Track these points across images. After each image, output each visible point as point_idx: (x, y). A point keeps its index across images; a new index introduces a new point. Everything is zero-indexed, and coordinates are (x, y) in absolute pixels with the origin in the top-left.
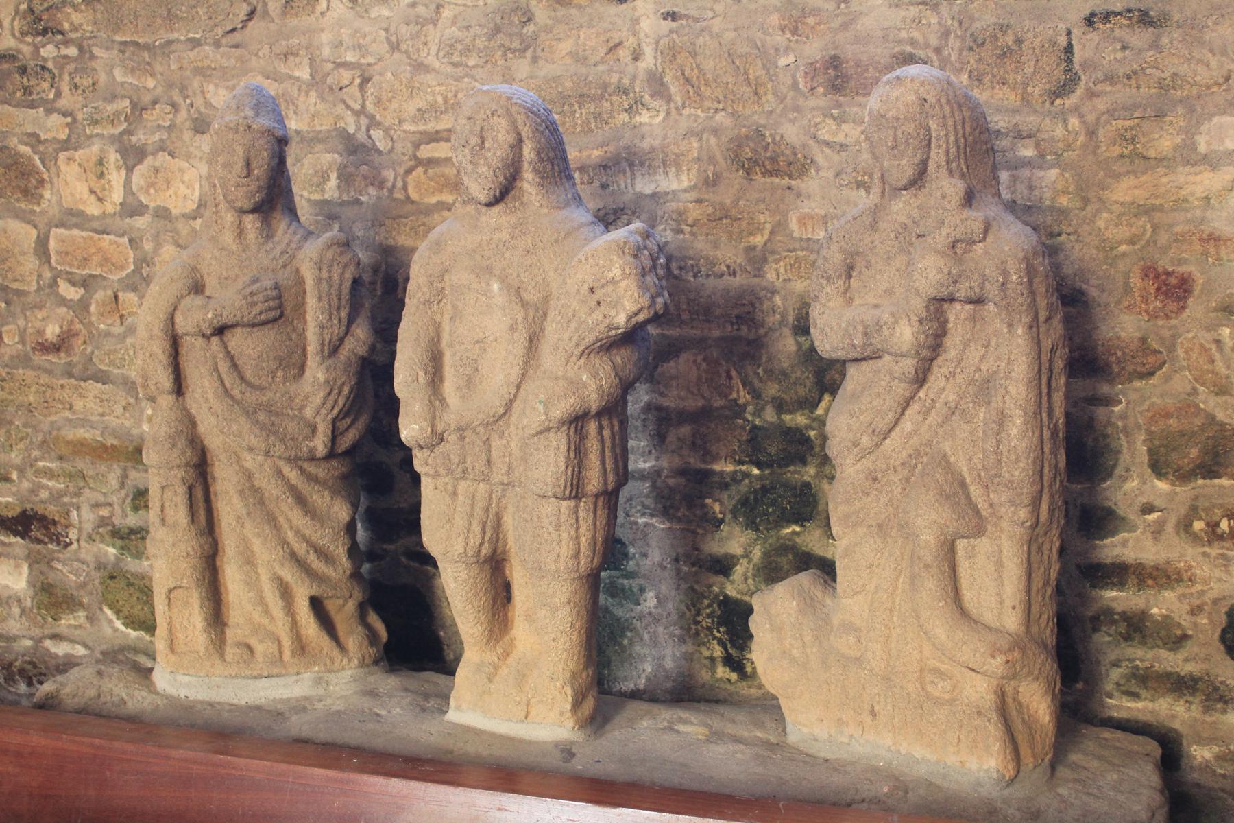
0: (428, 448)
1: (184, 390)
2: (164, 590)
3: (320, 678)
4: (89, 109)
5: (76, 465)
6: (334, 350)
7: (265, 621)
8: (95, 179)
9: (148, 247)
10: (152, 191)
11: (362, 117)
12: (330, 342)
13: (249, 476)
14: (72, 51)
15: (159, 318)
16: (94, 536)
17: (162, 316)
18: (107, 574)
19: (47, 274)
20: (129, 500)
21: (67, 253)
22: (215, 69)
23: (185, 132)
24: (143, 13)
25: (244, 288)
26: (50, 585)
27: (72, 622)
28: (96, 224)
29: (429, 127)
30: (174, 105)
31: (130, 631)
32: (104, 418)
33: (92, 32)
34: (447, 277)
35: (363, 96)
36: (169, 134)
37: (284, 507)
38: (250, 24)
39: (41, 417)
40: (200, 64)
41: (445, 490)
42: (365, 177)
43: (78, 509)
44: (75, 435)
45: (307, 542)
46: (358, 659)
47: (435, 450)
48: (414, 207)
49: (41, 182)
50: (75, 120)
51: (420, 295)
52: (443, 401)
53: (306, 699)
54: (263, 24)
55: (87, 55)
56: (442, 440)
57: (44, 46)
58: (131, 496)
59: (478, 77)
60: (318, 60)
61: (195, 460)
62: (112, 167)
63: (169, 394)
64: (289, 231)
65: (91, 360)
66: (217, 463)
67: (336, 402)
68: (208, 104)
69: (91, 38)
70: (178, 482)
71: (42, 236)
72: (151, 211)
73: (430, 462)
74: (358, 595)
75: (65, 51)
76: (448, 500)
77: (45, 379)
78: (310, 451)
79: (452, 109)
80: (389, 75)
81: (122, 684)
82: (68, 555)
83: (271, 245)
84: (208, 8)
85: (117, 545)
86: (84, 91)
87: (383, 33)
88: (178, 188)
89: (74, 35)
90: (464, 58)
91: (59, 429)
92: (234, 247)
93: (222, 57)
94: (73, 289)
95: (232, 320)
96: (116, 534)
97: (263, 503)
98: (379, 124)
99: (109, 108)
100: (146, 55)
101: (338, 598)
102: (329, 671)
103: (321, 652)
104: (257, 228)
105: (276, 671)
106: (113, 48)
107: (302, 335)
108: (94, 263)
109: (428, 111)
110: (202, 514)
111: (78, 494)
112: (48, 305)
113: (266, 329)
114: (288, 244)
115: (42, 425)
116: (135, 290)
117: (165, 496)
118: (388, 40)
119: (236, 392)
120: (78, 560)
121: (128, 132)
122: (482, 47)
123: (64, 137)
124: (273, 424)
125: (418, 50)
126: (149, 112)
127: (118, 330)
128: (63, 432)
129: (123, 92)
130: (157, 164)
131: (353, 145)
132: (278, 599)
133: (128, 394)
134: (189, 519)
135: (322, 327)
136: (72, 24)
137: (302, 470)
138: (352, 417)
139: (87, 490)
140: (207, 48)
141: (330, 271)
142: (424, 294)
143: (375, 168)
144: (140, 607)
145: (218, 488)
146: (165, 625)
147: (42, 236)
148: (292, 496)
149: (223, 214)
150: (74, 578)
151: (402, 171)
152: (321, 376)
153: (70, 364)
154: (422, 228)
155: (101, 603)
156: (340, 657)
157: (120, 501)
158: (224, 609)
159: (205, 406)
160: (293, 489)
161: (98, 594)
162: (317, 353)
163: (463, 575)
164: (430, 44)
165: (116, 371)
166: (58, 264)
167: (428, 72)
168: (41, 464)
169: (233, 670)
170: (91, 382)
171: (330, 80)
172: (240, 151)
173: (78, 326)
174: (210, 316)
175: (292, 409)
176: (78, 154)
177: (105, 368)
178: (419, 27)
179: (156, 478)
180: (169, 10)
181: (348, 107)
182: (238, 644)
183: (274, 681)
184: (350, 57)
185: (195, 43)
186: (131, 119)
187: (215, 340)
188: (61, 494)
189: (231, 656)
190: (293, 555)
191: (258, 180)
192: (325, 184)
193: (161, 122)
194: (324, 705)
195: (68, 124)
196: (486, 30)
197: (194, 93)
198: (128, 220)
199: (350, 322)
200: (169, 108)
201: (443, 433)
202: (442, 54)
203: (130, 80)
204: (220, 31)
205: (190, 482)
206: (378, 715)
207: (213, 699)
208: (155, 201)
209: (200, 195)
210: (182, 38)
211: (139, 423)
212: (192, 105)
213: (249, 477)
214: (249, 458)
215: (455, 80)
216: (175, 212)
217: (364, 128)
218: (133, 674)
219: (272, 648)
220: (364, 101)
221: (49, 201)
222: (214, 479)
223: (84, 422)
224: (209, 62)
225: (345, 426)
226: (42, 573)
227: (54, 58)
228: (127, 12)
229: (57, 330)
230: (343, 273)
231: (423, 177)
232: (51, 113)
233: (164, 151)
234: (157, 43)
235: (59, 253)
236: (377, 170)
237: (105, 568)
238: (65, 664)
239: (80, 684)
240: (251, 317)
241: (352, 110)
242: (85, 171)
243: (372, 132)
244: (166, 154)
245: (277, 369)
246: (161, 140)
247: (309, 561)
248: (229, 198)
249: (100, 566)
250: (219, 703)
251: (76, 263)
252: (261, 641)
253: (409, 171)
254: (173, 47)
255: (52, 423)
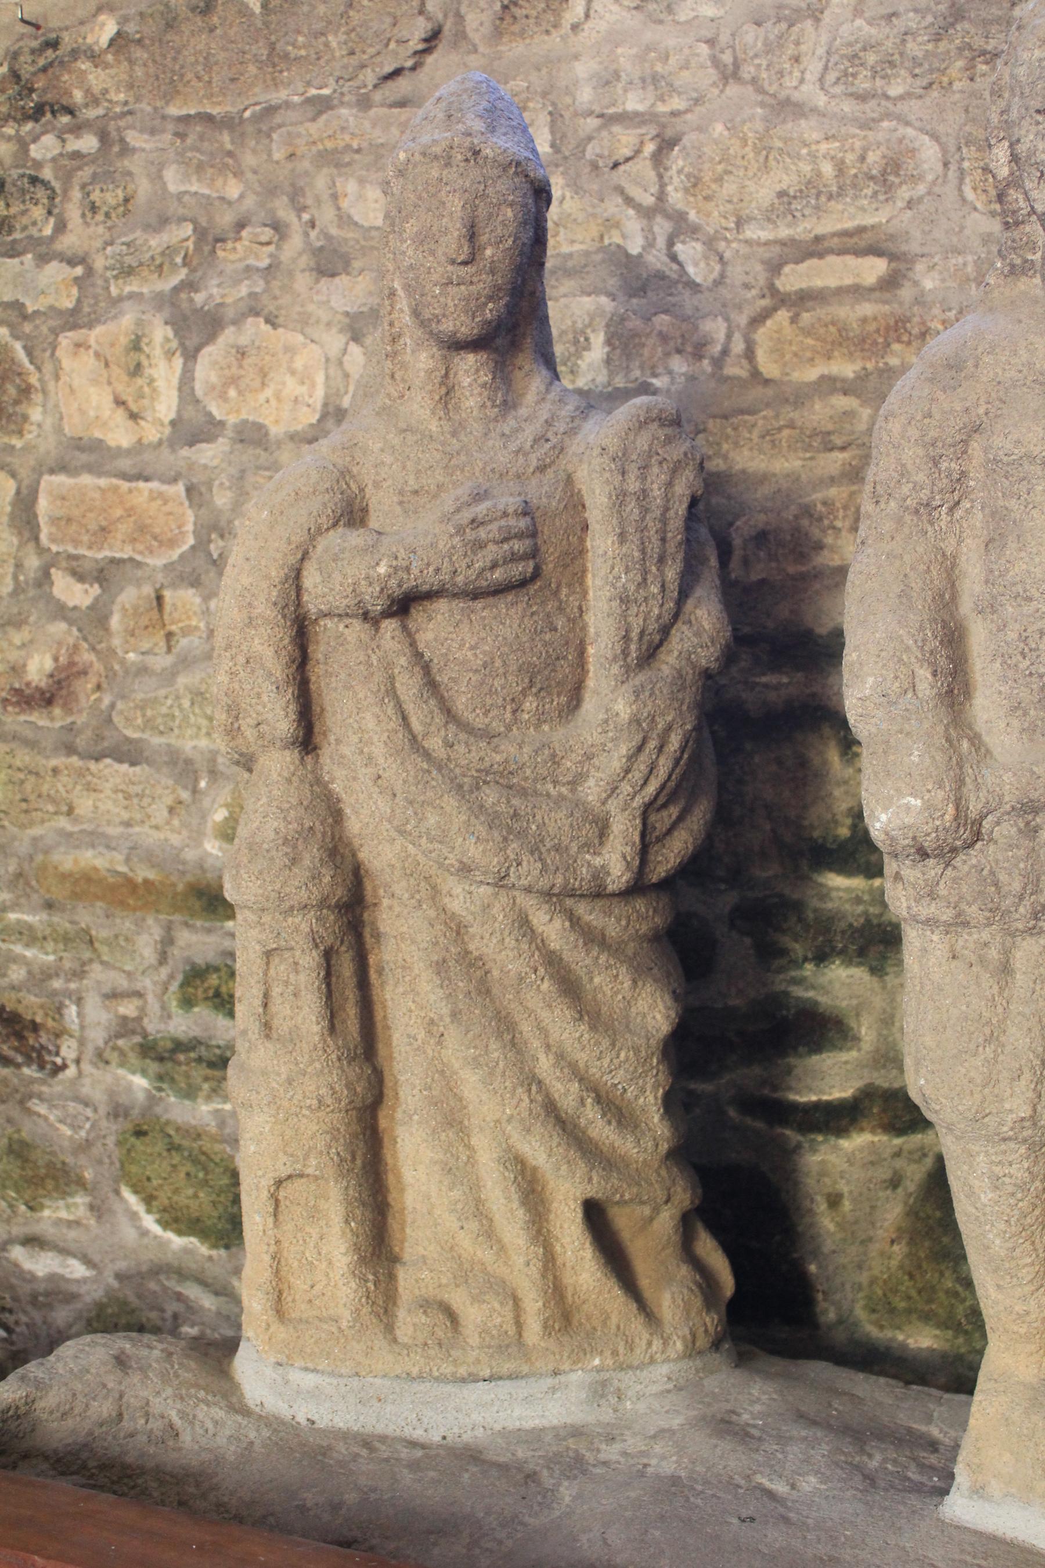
0: (940, 856)
1: (318, 739)
2: (267, 1182)
3: (604, 1384)
4: (117, 248)
5: (77, 918)
6: (650, 655)
7: (486, 1255)
8: (126, 378)
9: (222, 499)
10: (232, 393)
11: (659, 219)
12: (642, 633)
13: (458, 930)
14: (88, 143)
15: (267, 577)
16: (107, 1054)
17: (276, 574)
18: (129, 1126)
19: (33, 562)
20: (174, 986)
21: (69, 520)
22: (358, 151)
23: (299, 276)
24: (222, 56)
25: (458, 510)
26: (24, 1144)
27: (63, 1214)
28: (125, 464)
29: (800, 229)
30: (278, 227)
31: (170, 1235)
32: (131, 830)
33: (126, 103)
34: (976, 447)
35: (660, 177)
36: (267, 282)
37: (533, 1000)
38: (430, 59)
39: (15, 830)
40: (329, 145)
41: (982, 960)
42: (664, 338)
43: (79, 1001)
44: (76, 861)
45: (581, 1080)
46: (684, 1338)
47: (957, 862)
48: (770, 392)
49: (26, 391)
50: (90, 271)
51: (906, 489)
52: (976, 740)
53: (577, 1432)
54: (454, 57)
55: (116, 149)
56: (978, 836)
57: (35, 140)
58: (180, 977)
59: (912, 118)
60: (567, 115)
61: (339, 892)
62: (158, 352)
63: (286, 747)
64: (551, 396)
65: (109, 720)
66: (386, 902)
67: (652, 769)
68: (345, 220)
69: (124, 114)
70: (300, 942)
71: (24, 491)
72: (229, 432)
73: (942, 890)
74: (684, 1196)
75: (75, 144)
76: (989, 984)
77: (23, 757)
78: (595, 877)
79: (854, 186)
80: (719, 128)
81: (169, 1391)
82: (58, 1089)
83: (512, 423)
84: (347, 33)
85: (151, 1072)
86: (107, 215)
87: (704, 49)
88: (284, 383)
89: (92, 113)
90: (879, 82)
91: (46, 852)
92: (434, 427)
93: (374, 126)
94: (79, 587)
95: (430, 580)
96: (149, 1050)
97: (488, 992)
98: (694, 230)
99: (153, 243)
100: (226, 138)
101: (643, 1203)
102: (621, 1367)
103: (604, 1323)
104: (484, 385)
105: (507, 1367)
106: (163, 131)
107: (577, 621)
108: (119, 536)
109: (800, 196)
110: (351, 1012)
111: (79, 974)
112: (32, 619)
113: (502, 604)
114: (548, 423)
115: (16, 843)
116: (195, 583)
117: (272, 972)
118: (716, 62)
119: (434, 744)
120: (77, 1099)
121: (190, 286)
122: (920, 54)
123: (69, 304)
124: (515, 815)
125: (781, 74)
126: (230, 245)
127: (161, 661)
128: (56, 857)
129: (181, 211)
130: (243, 340)
131: (638, 277)
132: (515, 1205)
133: (176, 782)
134: (326, 1023)
135: (625, 600)
136: (88, 91)
137: (574, 921)
138: (682, 803)
139: (96, 967)
140: (344, 111)
141: (643, 478)
142: (917, 487)
143: (685, 319)
144: (190, 1192)
145: (386, 957)
146: (267, 1258)
147: (24, 491)
148: (552, 977)
149: (408, 358)
150: (69, 1133)
151: (743, 320)
152: (623, 709)
153: (70, 728)
154: (786, 432)
155: (117, 1181)
156: (646, 1336)
157: (159, 990)
158: (393, 1224)
159: (365, 774)
160: (553, 962)
161: (112, 1163)
162: (615, 658)
163: (1018, 1172)
164: (804, 60)
165: (157, 740)
166: (53, 540)
167: (803, 115)
168: (13, 916)
169: (415, 1363)
170: (108, 761)
171: (590, 152)
172: (456, 205)
173: (87, 657)
174: (382, 570)
175: (555, 783)
176: (95, 335)
177: (136, 735)
178: (784, 26)
179: (254, 933)
180: (272, 47)
181: (629, 201)
182: (425, 1305)
183: (504, 1388)
184: (634, 103)
185: (321, 106)
186: (195, 263)
187: (390, 626)
188: (48, 974)
189: (410, 1331)
190: (551, 1109)
191: (492, 272)
192: (580, 357)
193: (251, 261)
194: (625, 1454)
195: (77, 280)
196: (930, 19)
197: (318, 201)
198: (185, 452)
199: (684, 594)
200: (267, 234)
201: (983, 817)
202: (831, 77)
203: (194, 189)
204: (369, 77)
205: (329, 941)
206: (771, 1495)
207: (369, 1429)
208: (238, 411)
209: (327, 396)
210: (296, 99)
211: (197, 837)
212: (312, 224)
213: (458, 933)
214: (458, 890)
215: (861, 128)
216: (275, 431)
217: (661, 242)
218: (193, 1364)
219: (502, 1317)
220: (662, 186)
221: (39, 426)
222: (377, 936)
223: (94, 838)
224: (347, 137)
225: (668, 823)
226: (9, 1120)
227: (54, 160)
228: (192, 59)
229: (49, 665)
230: (670, 484)
231: (788, 330)
232: (48, 262)
233: (257, 314)
234: (247, 114)
235: (54, 521)
236: (689, 321)
237: (126, 1116)
238: (47, 1294)
239: (79, 1387)
240: (472, 574)
241: (638, 207)
242: (107, 365)
243: (679, 247)
244: (261, 320)
245: (524, 693)
246: (252, 295)
247: (583, 1122)
248: (427, 314)
249: (118, 1111)
250: (383, 1439)
251: (85, 538)
252: (476, 1299)
253: (758, 320)
254: (278, 119)
255: (35, 840)
